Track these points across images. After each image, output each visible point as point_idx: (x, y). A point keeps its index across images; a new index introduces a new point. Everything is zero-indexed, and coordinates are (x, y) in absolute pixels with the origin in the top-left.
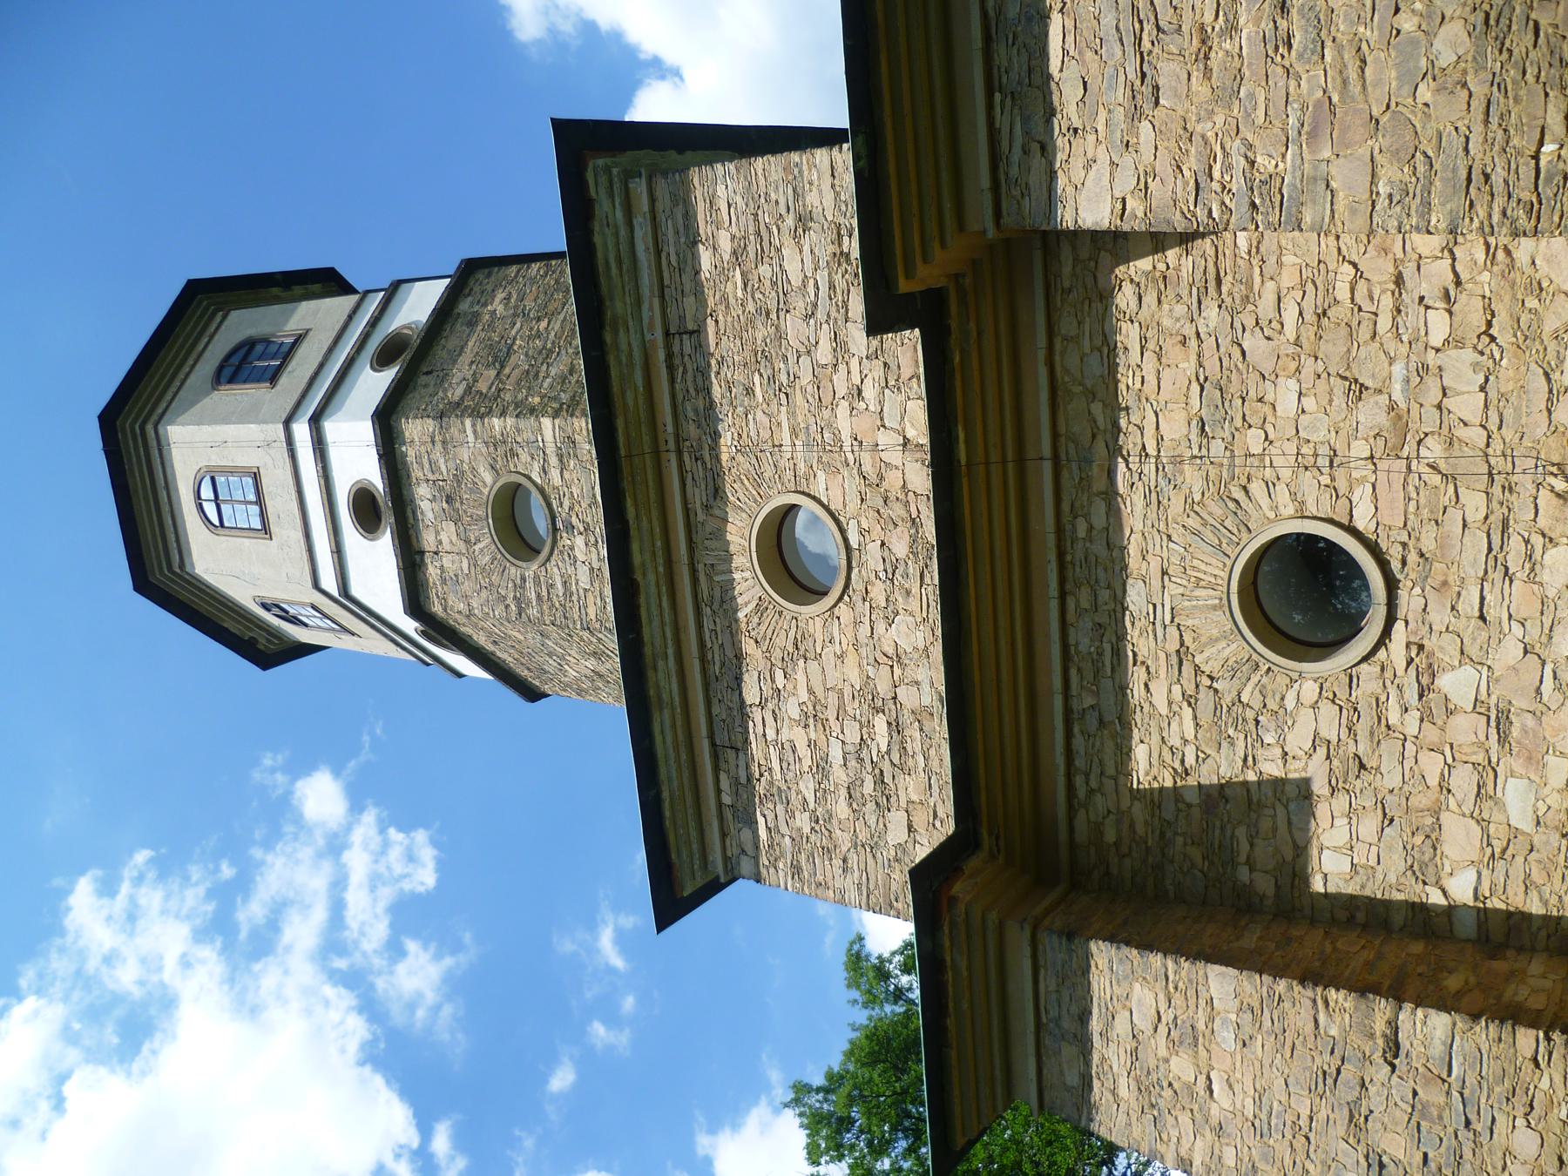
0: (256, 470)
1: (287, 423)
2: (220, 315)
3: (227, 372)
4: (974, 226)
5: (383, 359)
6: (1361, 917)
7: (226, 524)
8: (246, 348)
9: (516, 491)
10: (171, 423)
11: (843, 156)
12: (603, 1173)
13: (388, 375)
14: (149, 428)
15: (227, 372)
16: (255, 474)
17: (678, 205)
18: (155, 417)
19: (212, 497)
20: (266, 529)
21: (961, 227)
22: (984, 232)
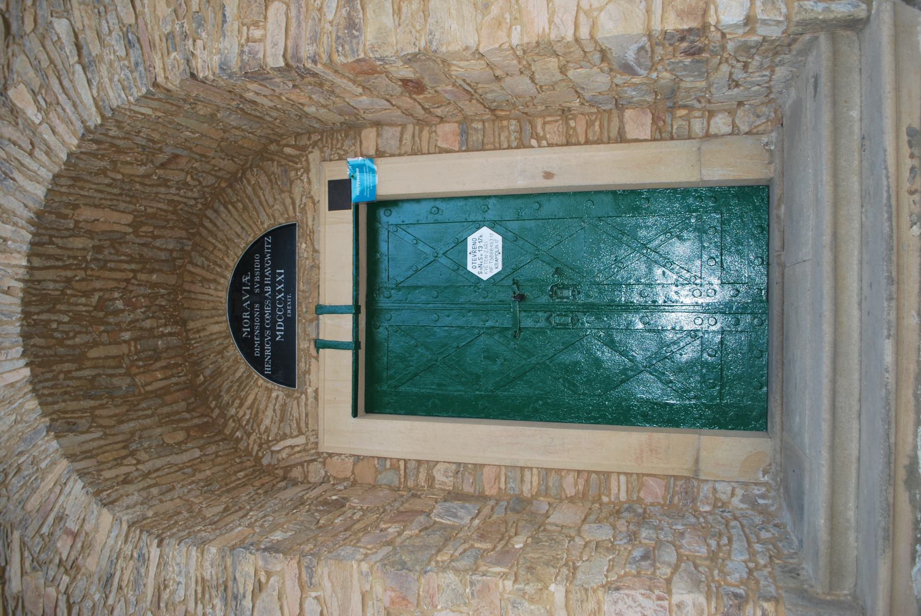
11: (348, 355)
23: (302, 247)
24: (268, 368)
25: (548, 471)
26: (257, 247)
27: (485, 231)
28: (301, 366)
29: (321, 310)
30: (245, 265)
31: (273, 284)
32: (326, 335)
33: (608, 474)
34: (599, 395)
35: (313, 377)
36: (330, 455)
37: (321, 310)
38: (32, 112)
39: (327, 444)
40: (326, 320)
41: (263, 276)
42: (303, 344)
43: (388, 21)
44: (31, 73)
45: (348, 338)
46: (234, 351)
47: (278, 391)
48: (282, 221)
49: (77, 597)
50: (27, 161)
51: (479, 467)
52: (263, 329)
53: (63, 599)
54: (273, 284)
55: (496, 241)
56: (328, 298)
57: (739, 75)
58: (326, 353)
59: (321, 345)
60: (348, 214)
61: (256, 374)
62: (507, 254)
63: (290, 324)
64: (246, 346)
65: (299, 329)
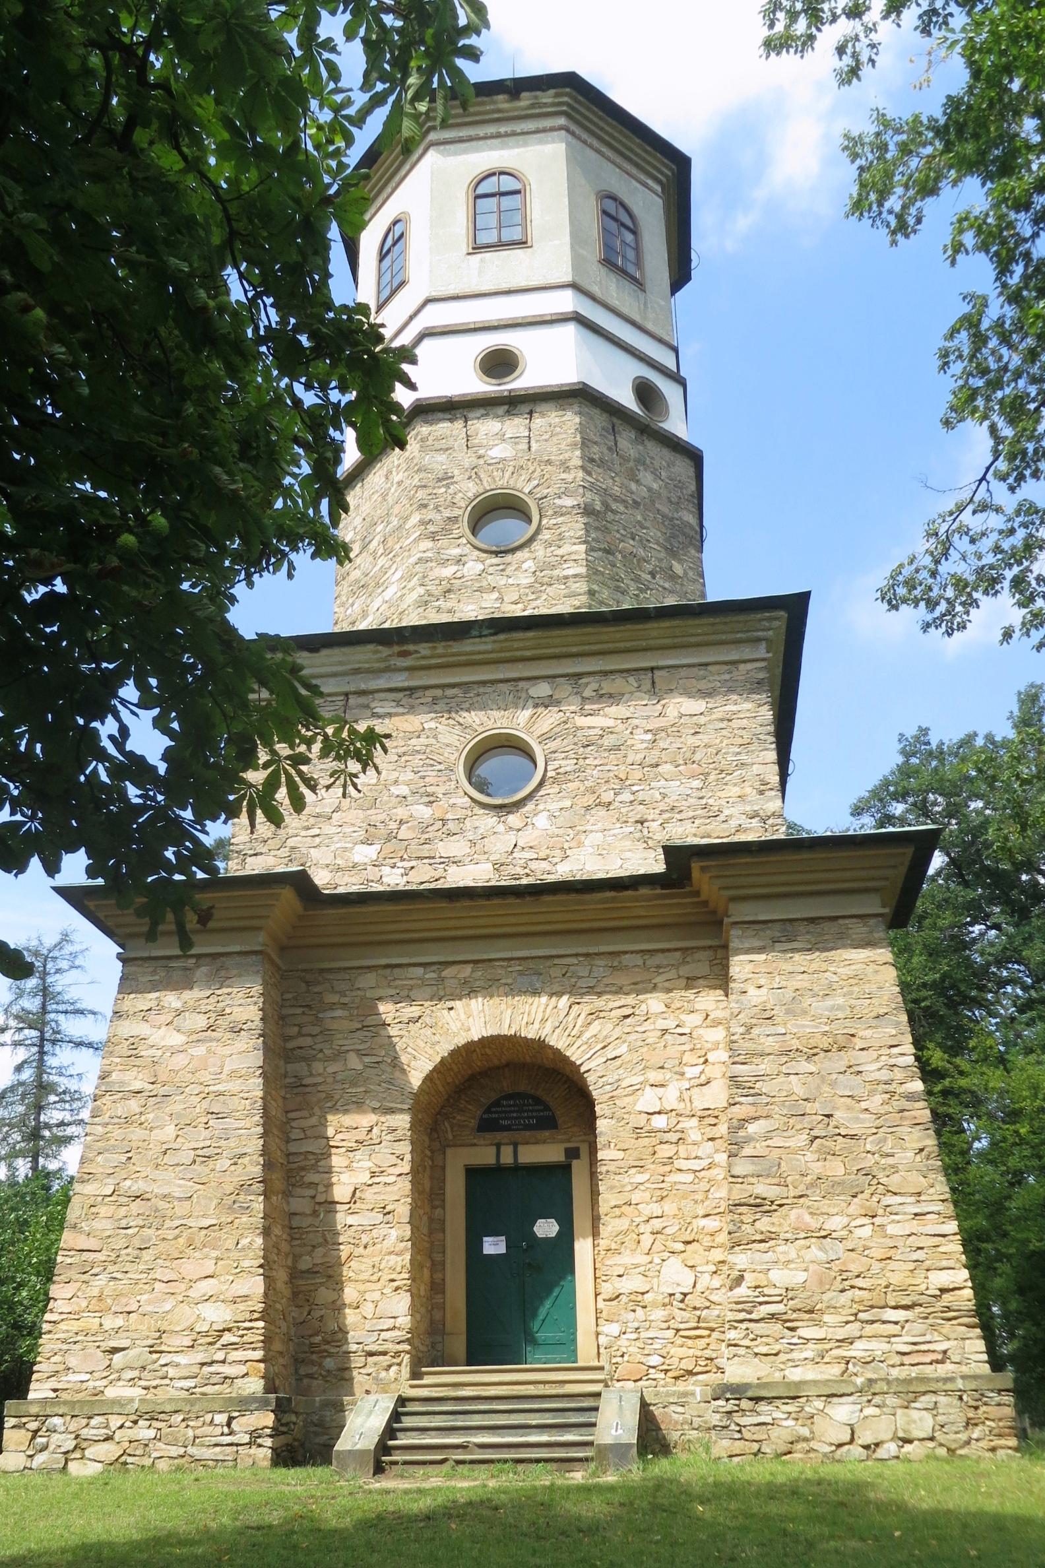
0: (529, 244)
1: (574, 286)
2: (658, 188)
3: (611, 206)
4: (733, 908)
5: (645, 392)
6: (299, 1204)
7: (478, 201)
8: (629, 223)
9: (514, 509)
10: (568, 145)
11: (494, 1162)
12: (272, 633)
13: (627, 398)
14: (562, 121)
15: (611, 206)
16: (525, 243)
17: (1024, 607)
18: (573, 127)
19: (494, 200)
20: (477, 248)
21: (733, 899)
22: (728, 916)
23: (547, 1133)
24: (486, 1116)
25: (444, 1265)
26: (547, 1108)
27: (556, 1228)
28: (488, 1135)
29: (515, 1145)
30: (538, 1101)
31: (528, 1118)
32: (503, 1148)
33: (444, 1293)
34: (657, 1542)
35: (482, 1142)
36: (444, 1153)
37: (515, 1145)
38: (587, 1035)
39: (449, 1151)
40: (510, 1149)
41: (532, 1111)
42: (499, 1136)
43: (613, 1204)
44: (604, 1033)
45: (502, 1161)
46: (494, 1096)
47: (474, 1123)
48: (560, 1122)
49: (382, 1066)
50: (567, 1033)
51: (444, 1231)
52: (505, 1112)
53: (380, 1059)
54: (528, 1118)
55: (355, 496)
56: (521, 1148)
57: (649, 567)
58: (494, 1149)
59: (498, 1146)
60: (563, 1159)
61: (482, 1110)
62: (547, 1239)
63: (508, 1128)
64: (497, 1103)
65: (505, 1133)
